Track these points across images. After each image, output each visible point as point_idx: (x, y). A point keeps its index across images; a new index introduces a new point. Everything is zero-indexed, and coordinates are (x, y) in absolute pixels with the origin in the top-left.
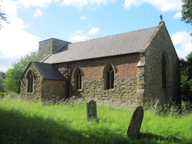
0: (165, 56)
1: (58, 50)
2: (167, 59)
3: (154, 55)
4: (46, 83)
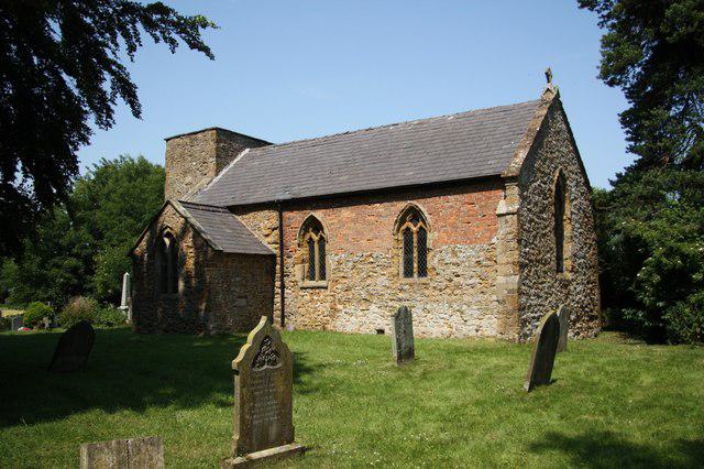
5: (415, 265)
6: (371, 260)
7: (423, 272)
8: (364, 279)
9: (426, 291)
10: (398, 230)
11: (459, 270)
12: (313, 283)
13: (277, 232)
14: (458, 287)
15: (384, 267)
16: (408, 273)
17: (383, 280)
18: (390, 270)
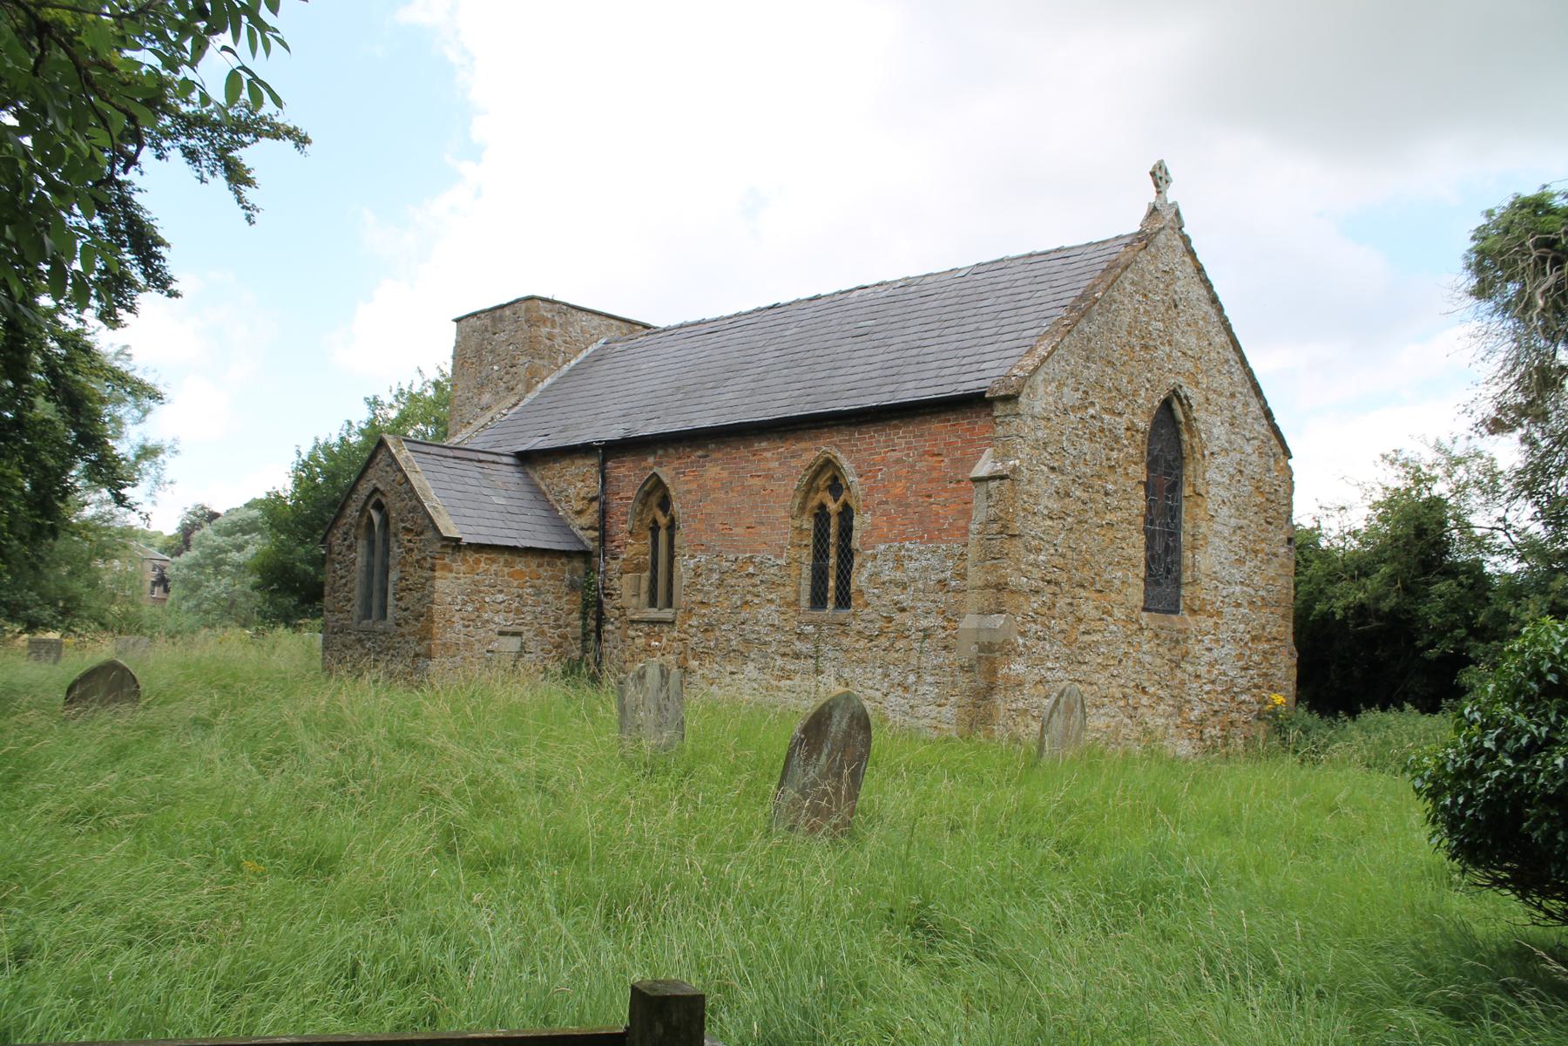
0: (1181, 417)
1: (566, 368)
2: (1192, 437)
3: (1091, 411)
4: (463, 568)
5: (832, 583)
6: (751, 570)
7: (844, 600)
8: (736, 609)
9: (846, 641)
10: (802, 508)
11: (905, 598)
12: (653, 613)
13: (596, 505)
14: (902, 634)
15: (773, 585)
16: (818, 600)
17: (768, 613)
18: (783, 591)
